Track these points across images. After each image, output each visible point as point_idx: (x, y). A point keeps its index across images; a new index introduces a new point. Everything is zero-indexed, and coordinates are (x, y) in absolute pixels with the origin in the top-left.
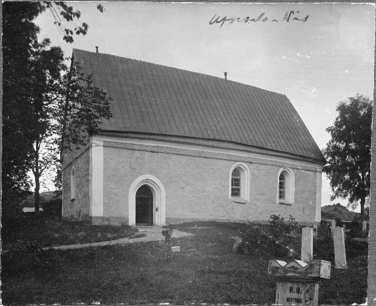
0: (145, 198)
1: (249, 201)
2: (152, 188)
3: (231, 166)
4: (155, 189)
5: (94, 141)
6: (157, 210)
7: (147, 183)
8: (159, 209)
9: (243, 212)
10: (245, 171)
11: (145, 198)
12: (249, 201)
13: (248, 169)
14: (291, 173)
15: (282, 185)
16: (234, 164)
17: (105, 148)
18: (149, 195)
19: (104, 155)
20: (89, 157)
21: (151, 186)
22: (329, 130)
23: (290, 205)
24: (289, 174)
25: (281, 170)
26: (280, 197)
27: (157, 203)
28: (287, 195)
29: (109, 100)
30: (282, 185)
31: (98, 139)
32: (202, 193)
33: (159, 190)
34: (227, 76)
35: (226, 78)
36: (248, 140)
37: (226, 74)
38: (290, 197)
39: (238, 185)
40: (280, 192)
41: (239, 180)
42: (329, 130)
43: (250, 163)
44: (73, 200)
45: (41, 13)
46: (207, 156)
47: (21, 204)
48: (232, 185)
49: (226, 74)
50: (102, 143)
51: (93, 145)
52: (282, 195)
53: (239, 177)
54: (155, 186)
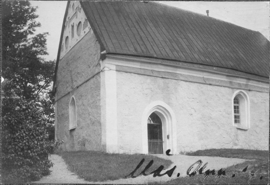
1: (249, 128)
4: (165, 117)
6: (168, 137)
8: (170, 137)
9: (246, 139)
12: (249, 128)
15: (236, 109)
17: (117, 72)
19: (117, 79)
20: (99, 83)
24: (245, 99)
27: (167, 130)
28: (242, 118)
30: (236, 109)
31: (111, 62)
32: (209, 120)
33: (168, 115)
34: (209, 13)
35: (208, 15)
36: (242, 68)
37: (208, 12)
39: (238, 112)
40: (235, 117)
45: (46, 44)
46: (211, 83)
47: (34, 25)
49: (208, 12)
50: (114, 68)
51: (106, 69)
52: (237, 119)
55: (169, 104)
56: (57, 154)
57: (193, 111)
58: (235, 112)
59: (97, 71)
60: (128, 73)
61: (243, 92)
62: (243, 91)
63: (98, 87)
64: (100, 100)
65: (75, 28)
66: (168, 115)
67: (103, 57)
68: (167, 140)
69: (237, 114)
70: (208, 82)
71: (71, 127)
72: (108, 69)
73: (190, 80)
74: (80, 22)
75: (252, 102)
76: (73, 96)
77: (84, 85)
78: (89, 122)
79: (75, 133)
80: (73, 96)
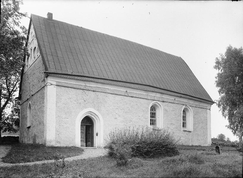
0: (88, 124)
2: (94, 119)
3: (149, 105)
5: (49, 81)
7: (90, 115)
10: (160, 107)
11: (88, 124)
13: (161, 105)
14: (191, 110)
15: (184, 118)
16: (152, 102)
18: (92, 124)
20: (44, 93)
21: (93, 117)
22: (50, 15)
23: (190, 132)
25: (184, 107)
26: (183, 126)
29: (71, 52)
30: (184, 118)
31: (52, 80)
33: (97, 118)
38: (190, 126)
41: (155, 114)
42: (50, 15)
43: (163, 102)
44: (29, 128)
48: (151, 110)
52: (184, 125)
53: (151, 118)
54: (95, 117)
55: (98, 110)
56: (103, 157)
57: (117, 116)
58: (151, 117)
59: (43, 85)
60: (66, 88)
61: (157, 103)
62: (157, 102)
63: (43, 98)
64: (44, 106)
65: (33, 50)
66: (97, 118)
67: (48, 74)
68: (97, 137)
69: (184, 121)
70: (130, 95)
71: (28, 126)
72: (50, 84)
73: (116, 93)
74: (35, 48)
75: (165, 110)
76: (30, 102)
77: (36, 94)
78: (38, 122)
79: (30, 130)
80: (30, 102)
